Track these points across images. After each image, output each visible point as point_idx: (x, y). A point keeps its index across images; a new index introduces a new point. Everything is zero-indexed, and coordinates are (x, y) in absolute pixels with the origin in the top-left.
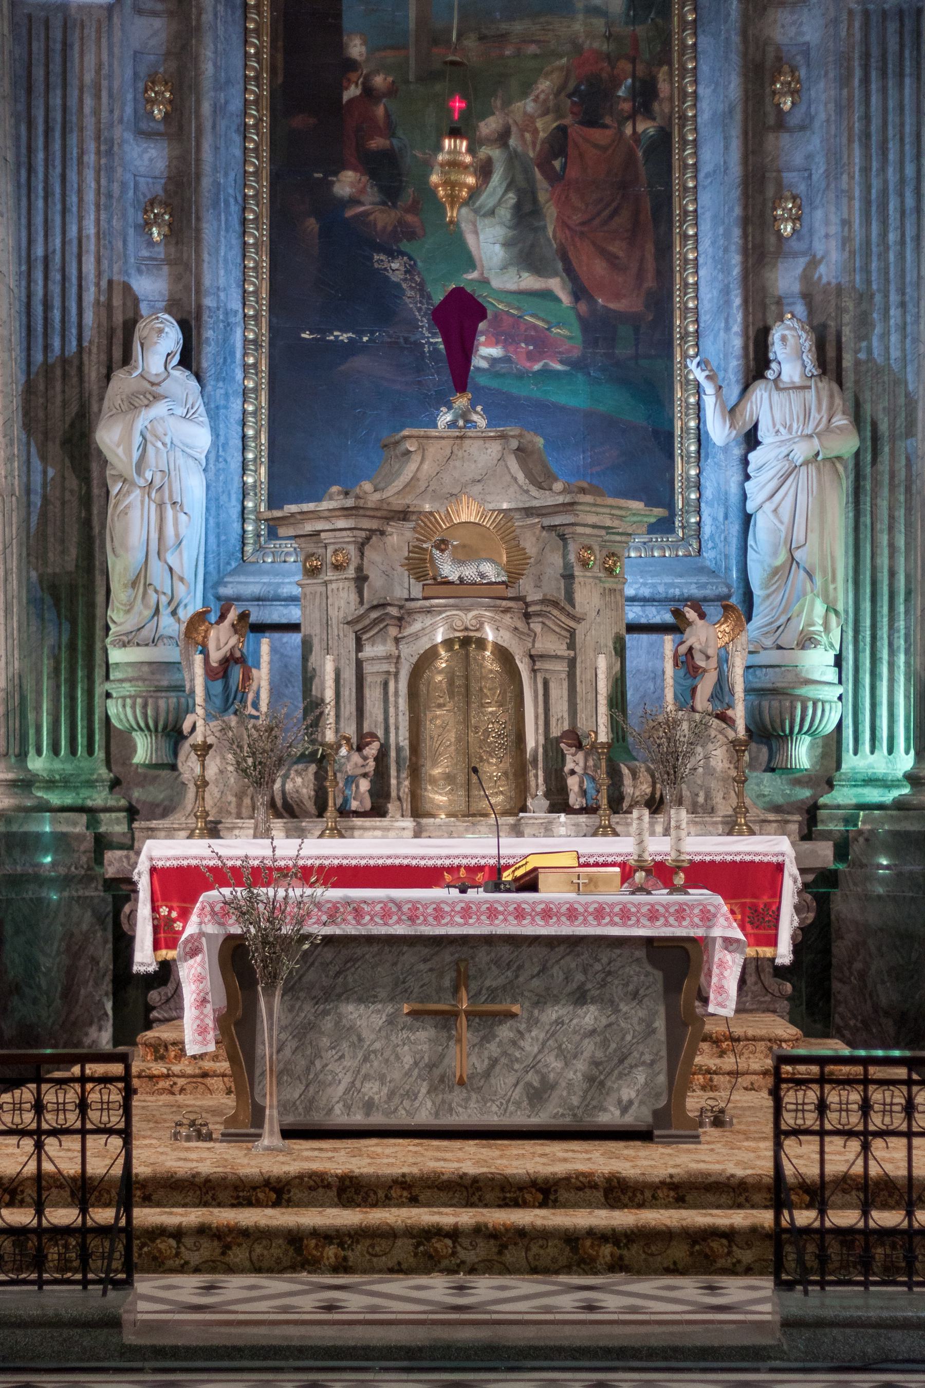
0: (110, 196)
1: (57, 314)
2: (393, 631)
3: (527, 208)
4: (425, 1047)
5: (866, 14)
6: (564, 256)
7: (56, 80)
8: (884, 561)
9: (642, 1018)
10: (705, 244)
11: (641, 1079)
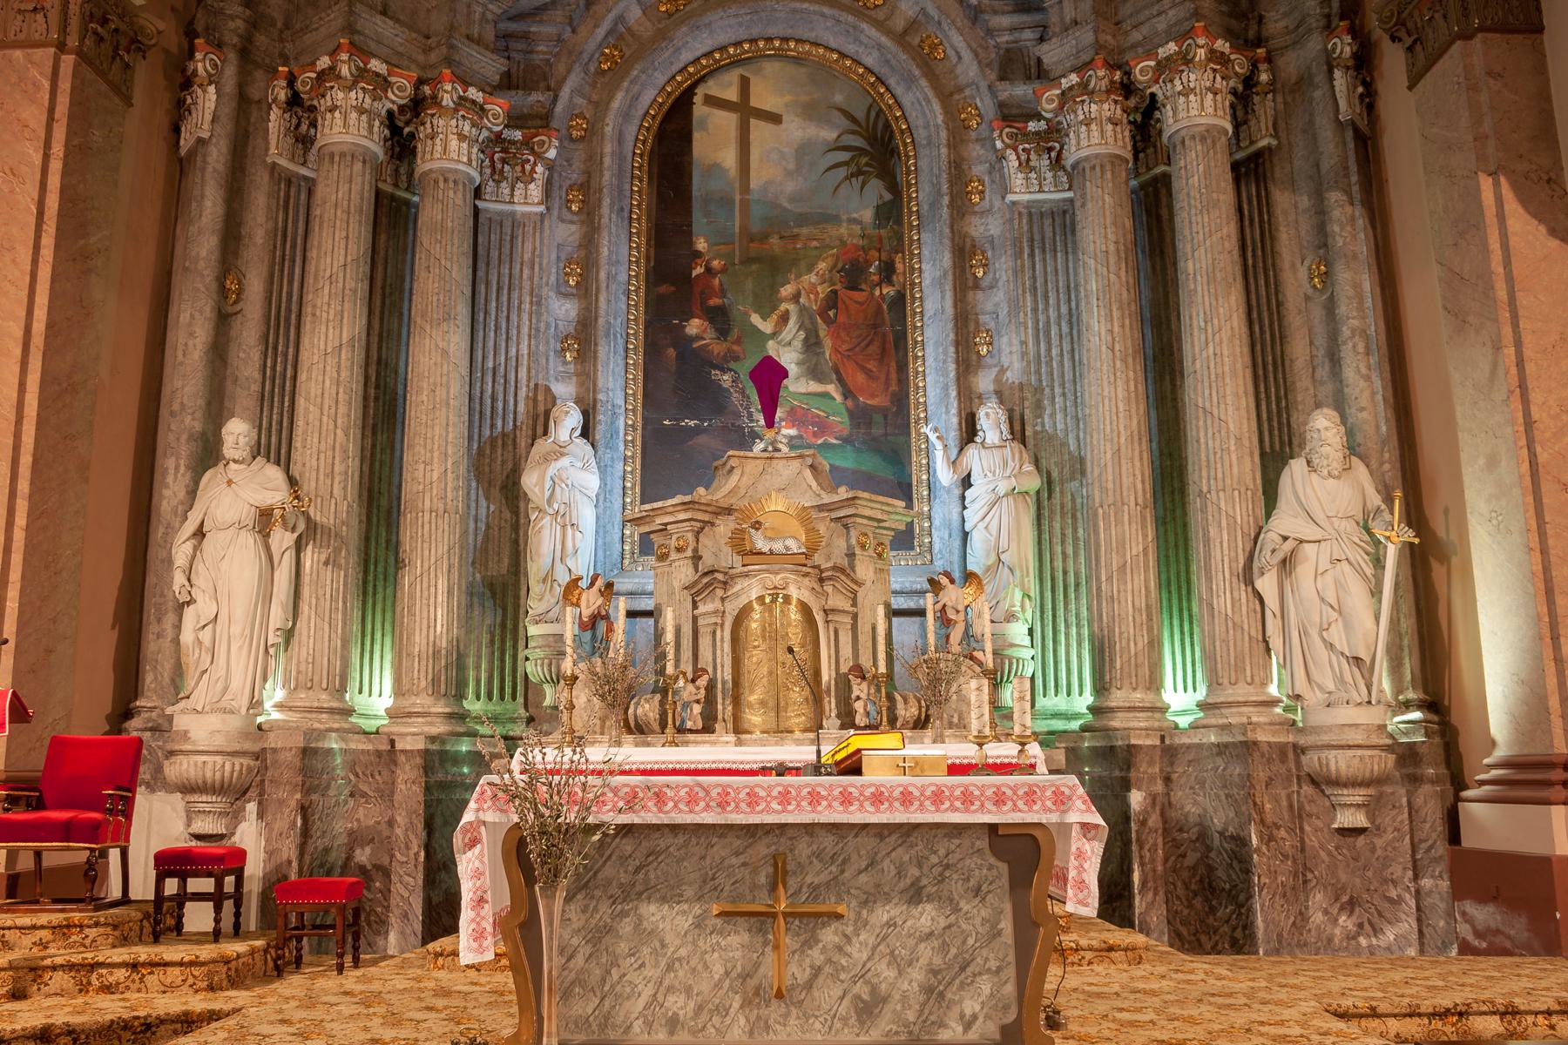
0: (538, 330)
1: (500, 405)
2: (719, 592)
3: (813, 341)
4: (738, 954)
5: (1030, 214)
6: (837, 372)
7: (505, 258)
8: (1059, 564)
9: (987, 916)
10: (930, 361)
11: (986, 988)
